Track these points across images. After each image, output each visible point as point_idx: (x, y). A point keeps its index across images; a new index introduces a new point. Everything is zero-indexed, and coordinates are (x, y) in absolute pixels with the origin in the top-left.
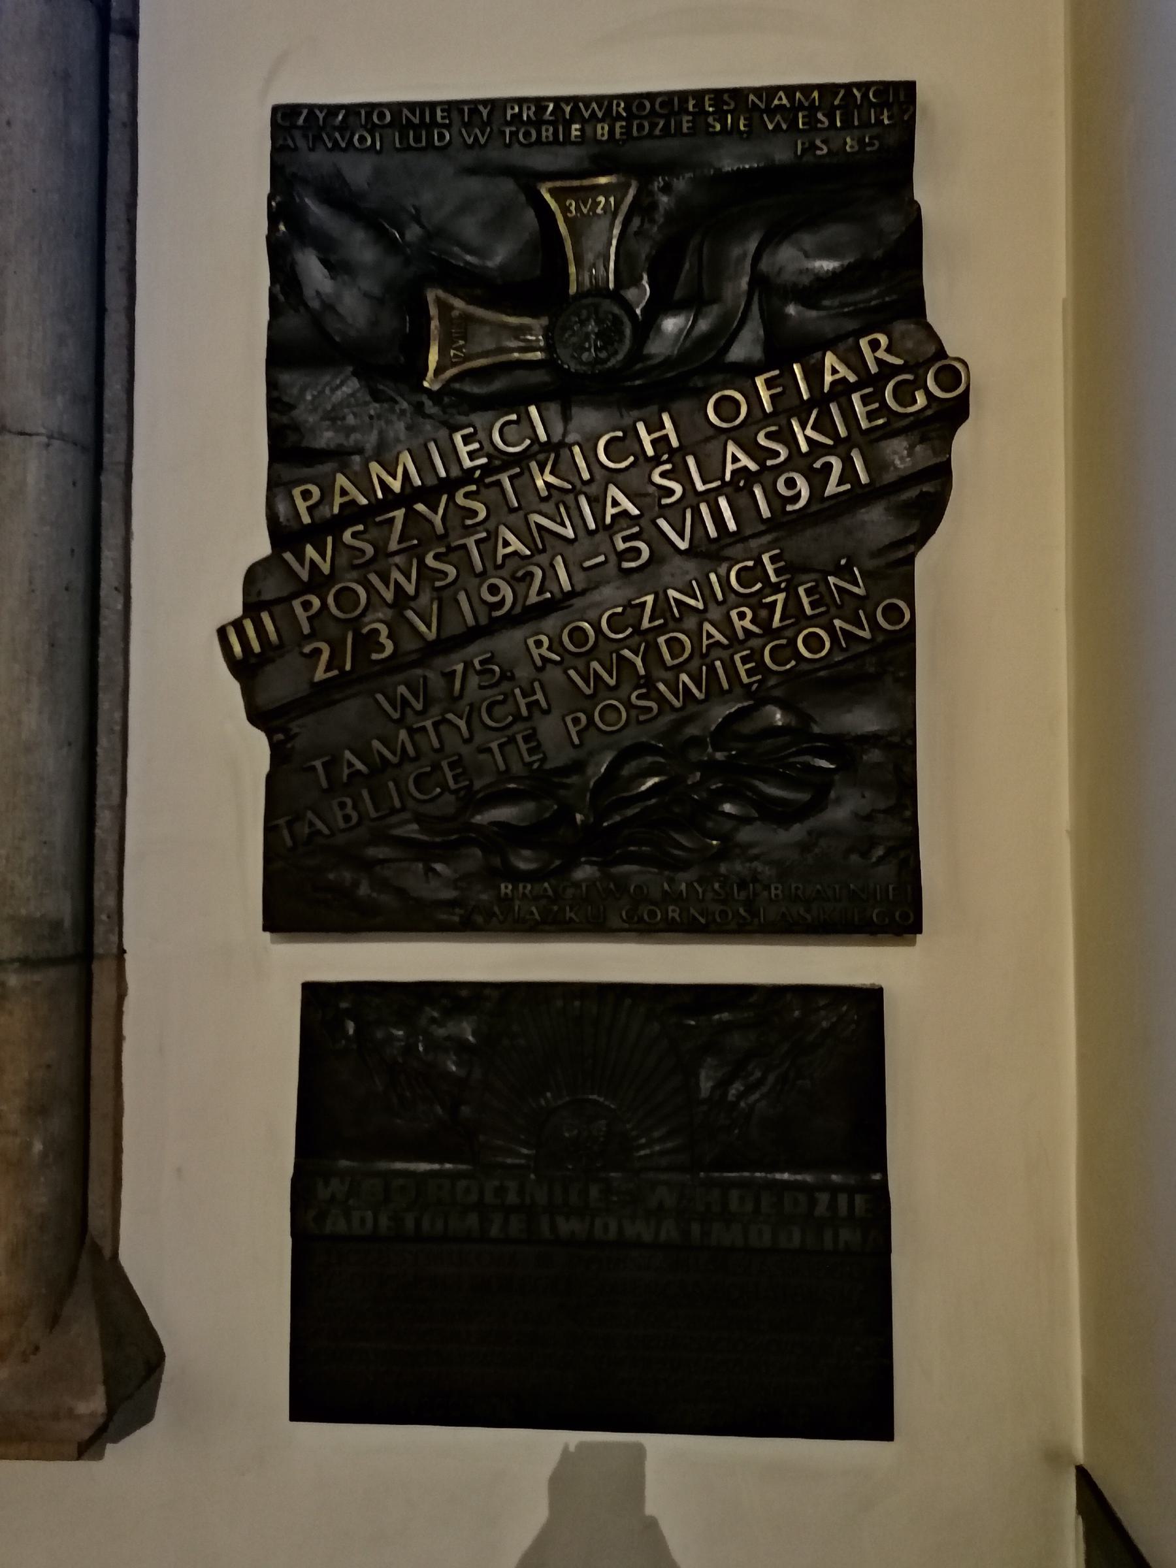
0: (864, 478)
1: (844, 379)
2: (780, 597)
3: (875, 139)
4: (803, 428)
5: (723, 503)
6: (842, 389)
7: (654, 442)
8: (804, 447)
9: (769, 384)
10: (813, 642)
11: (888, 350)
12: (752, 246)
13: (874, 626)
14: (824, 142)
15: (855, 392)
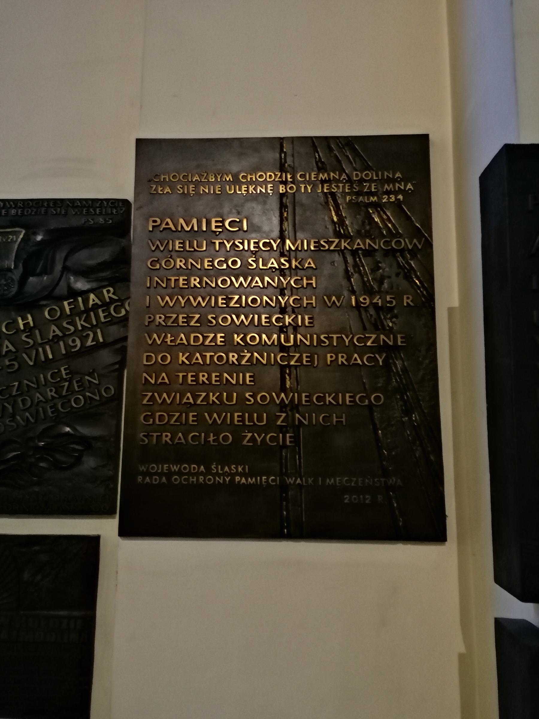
0: (101, 340)
1: (97, 304)
2: (67, 384)
3: (111, 220)
4: (80, 320)
5: (48, 348)
6: (95, 307)
7: (24, 324)
8: (80, 328)
9: (69, 304)
10: (77, 400)
11: (113, 294)
12: (64, 254)
13: (100, 395)
14: (92, 220)
15: (100, 308)
